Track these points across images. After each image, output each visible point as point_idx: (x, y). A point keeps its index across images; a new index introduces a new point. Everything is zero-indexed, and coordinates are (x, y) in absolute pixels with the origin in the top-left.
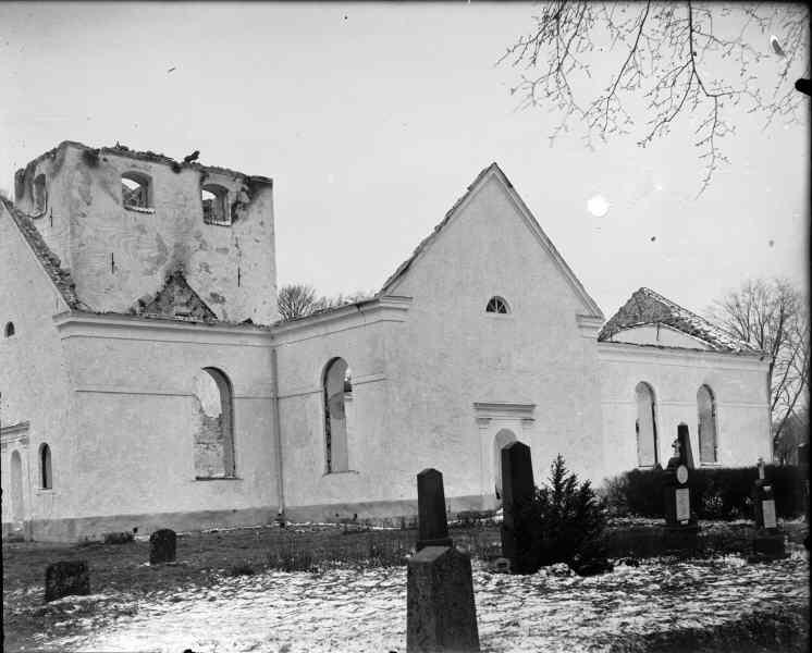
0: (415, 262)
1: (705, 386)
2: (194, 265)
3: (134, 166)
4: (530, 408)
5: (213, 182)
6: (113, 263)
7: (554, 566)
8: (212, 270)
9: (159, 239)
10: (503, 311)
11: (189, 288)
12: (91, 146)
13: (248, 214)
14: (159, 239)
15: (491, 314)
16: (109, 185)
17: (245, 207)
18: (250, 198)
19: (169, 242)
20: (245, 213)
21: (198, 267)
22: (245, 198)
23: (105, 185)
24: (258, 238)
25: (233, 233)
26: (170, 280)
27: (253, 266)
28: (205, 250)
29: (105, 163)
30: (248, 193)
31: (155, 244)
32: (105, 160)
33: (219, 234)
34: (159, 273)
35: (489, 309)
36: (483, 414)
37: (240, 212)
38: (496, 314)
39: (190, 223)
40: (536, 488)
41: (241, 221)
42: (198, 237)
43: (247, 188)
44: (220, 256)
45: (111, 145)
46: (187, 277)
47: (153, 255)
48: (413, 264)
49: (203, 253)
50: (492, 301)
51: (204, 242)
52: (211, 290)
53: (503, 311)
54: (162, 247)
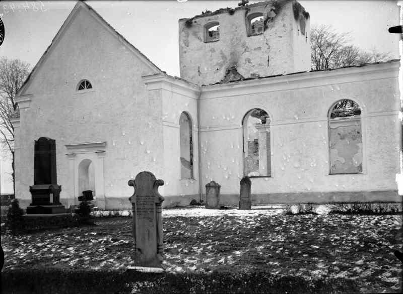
0: (33, 75)
1: (184, 112)
2: (242, 61)
3: (209, 20)
4: (103, 145)
5: (254, 12)
6: (199, 71)
7: (179, 292)
8: (251, 61)
9: (222, 53)
10: (90, 87)
11: (239, 74)
12: (187, 18)
13: (274, 24)
14: (222, 53)
15: (82, 91)
16: (197, 34)
17: (273, 19)
18: (276, 13)
19: (227, 53)
20: (272, 23)
21: (244, 62)
22: (273, 14)
23: (195, 34)
24: (281, 35)
25: (265, 37)
26: (228, 72)
27: (278, 52)
28: (248, 52)
29: (196, 24)
30: (274, 11)
31: (220, 55)
32: (195, 22)
33: (257, 40)
34: (222, 70)
35: (81, 88)
36: (71, 151)
37: (268, 24)
38: (86, 90)
39: (239, 40)
40: (22, 210)
41: (270, 28)
42: (243, 45)
43: (274, 8)
44: (256, 52)
45: (200, 14)
46: (238, 69)
47: (219, 62)
48: (31, 78)
49: (247, 53)
50: (83, 83)
51: (247, 47)
52: (251, 73)
53: (90, 87)
54: (224, 57)
